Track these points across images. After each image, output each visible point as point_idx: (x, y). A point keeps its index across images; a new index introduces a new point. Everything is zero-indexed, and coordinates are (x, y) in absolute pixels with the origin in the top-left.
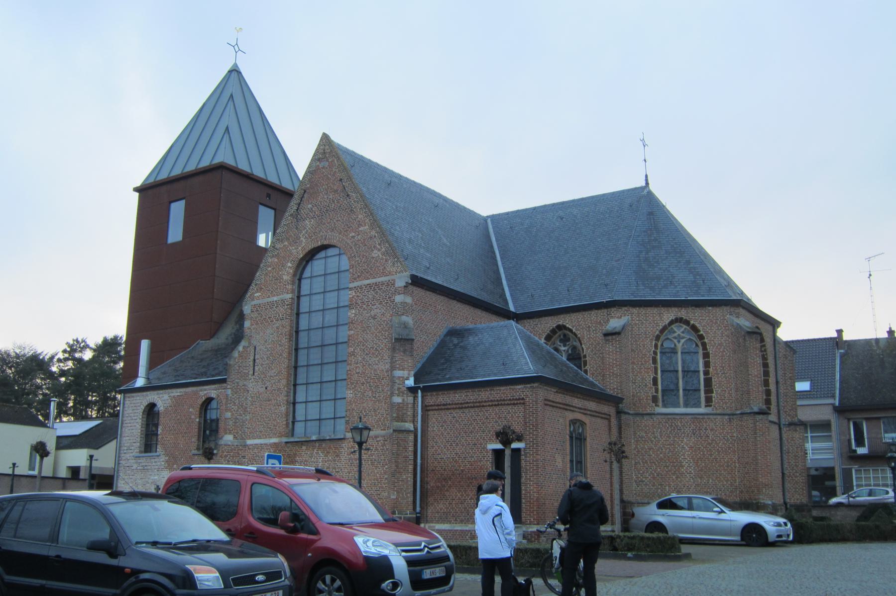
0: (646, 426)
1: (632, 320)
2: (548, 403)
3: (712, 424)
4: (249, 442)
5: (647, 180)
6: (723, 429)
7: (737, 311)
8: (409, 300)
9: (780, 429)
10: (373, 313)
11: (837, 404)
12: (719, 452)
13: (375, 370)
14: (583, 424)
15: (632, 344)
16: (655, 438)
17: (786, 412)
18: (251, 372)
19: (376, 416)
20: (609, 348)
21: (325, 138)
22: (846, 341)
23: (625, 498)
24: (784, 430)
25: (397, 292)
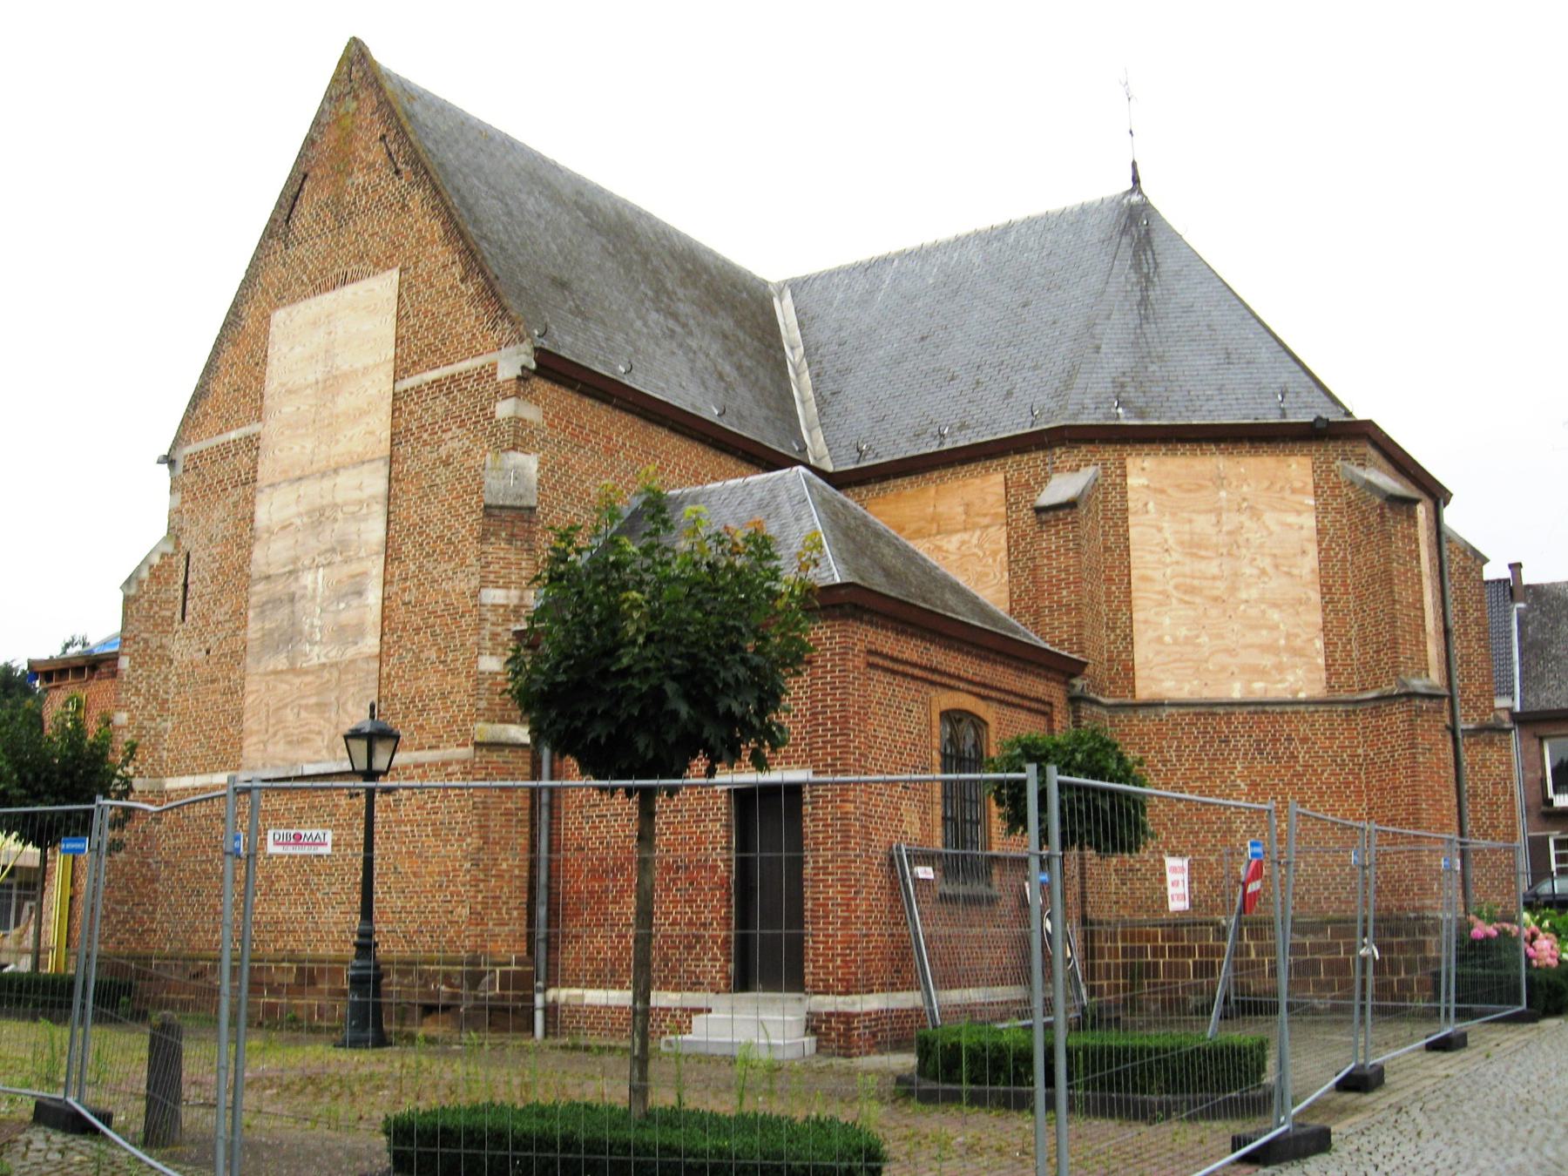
0: (1141, 734)
1: (1106, 475)
2: (878, 662)
3: (1304, 729)
4: (171, 783)
5: (1136, 180)
6: (1332, 738)
7: (1359, 450)
8: (532, 413)
9: (1455, 740)
10: (443, 451)
11: (1518, 709)
12: (1321, 794)
13: (446, 594)
14: (979, 723)
15: (1105, 534)
16: (1164, 762)
17: (1467, 702)
18: (178, 616)
19: (446, 709)
20: (1050, 541)
21: (356, 58)
22: (1528, 587)
23: (1092, 915)
24: (1464, 741)
25: (501, 393)
